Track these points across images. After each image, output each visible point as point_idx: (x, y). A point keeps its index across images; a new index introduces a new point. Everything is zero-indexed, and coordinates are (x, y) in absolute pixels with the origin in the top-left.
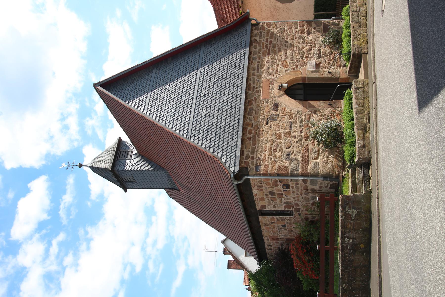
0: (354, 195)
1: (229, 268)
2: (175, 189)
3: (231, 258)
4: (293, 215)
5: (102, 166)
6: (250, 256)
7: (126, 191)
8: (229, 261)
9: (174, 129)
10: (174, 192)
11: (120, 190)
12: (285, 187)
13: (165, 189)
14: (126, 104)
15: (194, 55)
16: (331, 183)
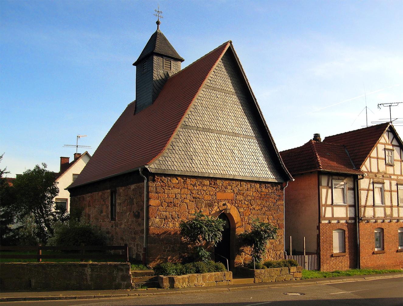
0: (131, 275)
1: (61, 158)
2: (135, 111)
3: (71, 160)
4: (111, 220)
5: (158, 43)
6: (74, 178)
7: (134, 65)
8: (68, 158)
9: (199, 98)
10: (133, 110)
11: (135, 60)
12: (137, 213)
13: (136, 101)
14: (220, 59)
15: (256, 131)
16: (141, 255)
